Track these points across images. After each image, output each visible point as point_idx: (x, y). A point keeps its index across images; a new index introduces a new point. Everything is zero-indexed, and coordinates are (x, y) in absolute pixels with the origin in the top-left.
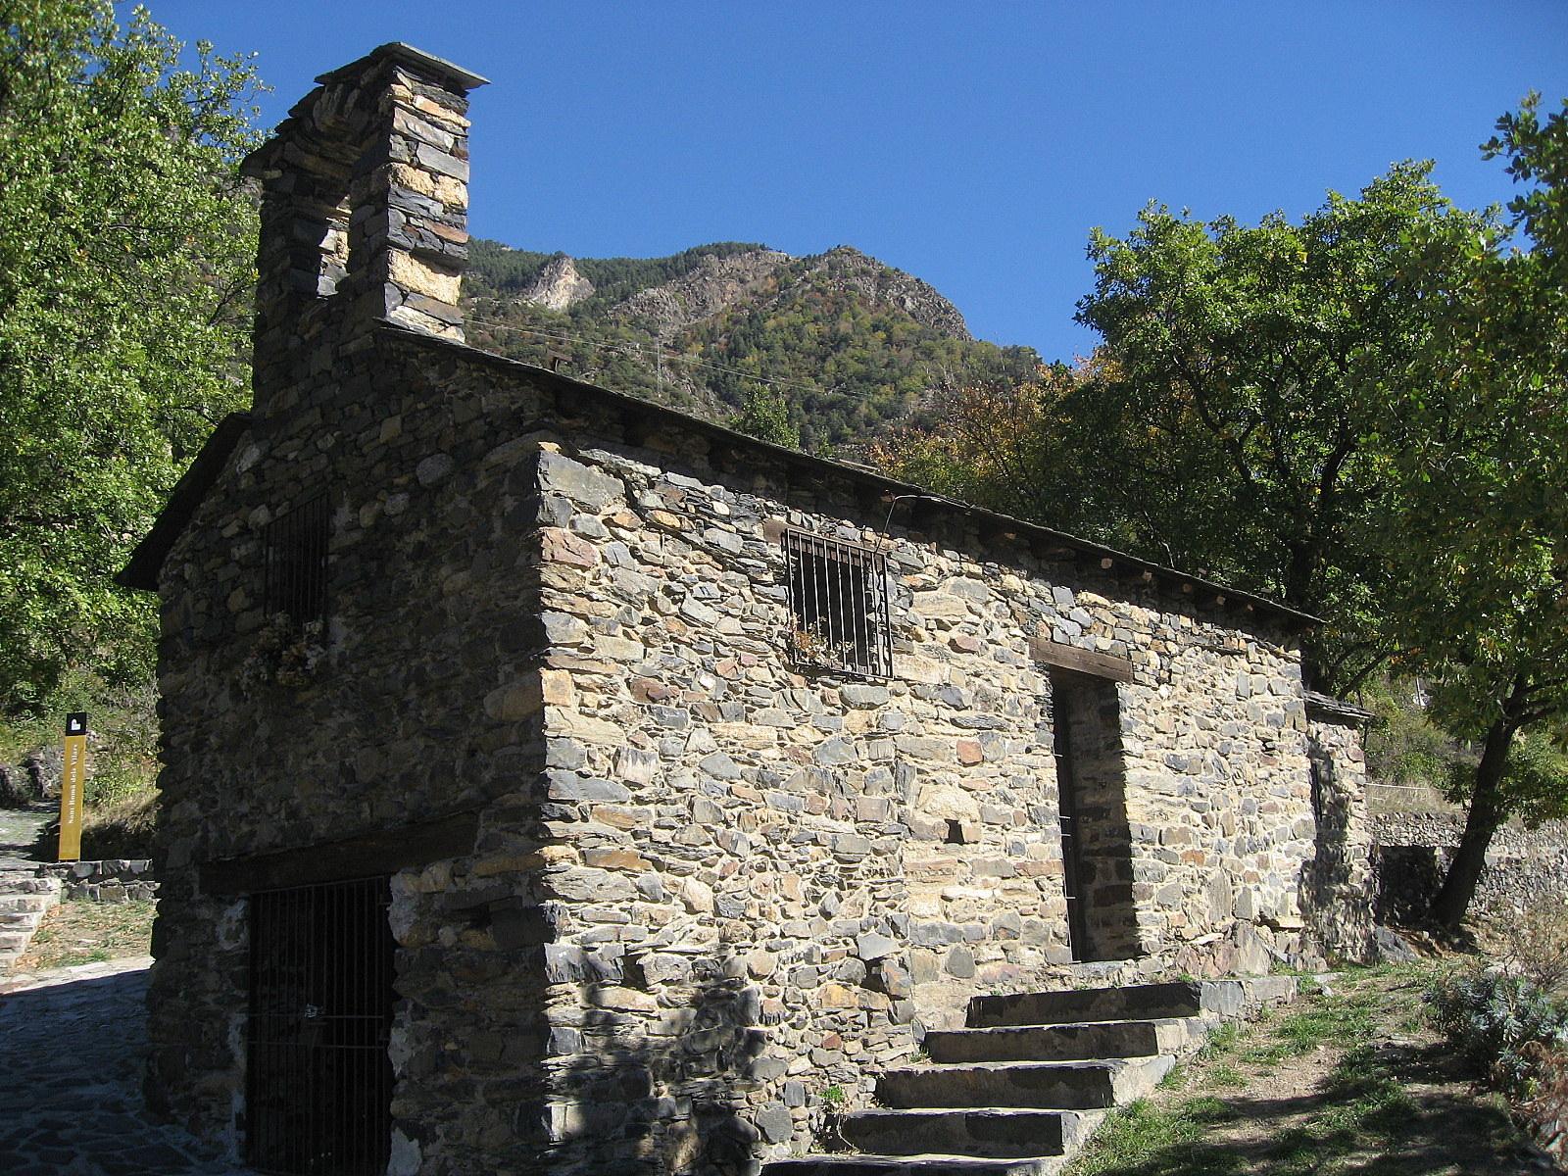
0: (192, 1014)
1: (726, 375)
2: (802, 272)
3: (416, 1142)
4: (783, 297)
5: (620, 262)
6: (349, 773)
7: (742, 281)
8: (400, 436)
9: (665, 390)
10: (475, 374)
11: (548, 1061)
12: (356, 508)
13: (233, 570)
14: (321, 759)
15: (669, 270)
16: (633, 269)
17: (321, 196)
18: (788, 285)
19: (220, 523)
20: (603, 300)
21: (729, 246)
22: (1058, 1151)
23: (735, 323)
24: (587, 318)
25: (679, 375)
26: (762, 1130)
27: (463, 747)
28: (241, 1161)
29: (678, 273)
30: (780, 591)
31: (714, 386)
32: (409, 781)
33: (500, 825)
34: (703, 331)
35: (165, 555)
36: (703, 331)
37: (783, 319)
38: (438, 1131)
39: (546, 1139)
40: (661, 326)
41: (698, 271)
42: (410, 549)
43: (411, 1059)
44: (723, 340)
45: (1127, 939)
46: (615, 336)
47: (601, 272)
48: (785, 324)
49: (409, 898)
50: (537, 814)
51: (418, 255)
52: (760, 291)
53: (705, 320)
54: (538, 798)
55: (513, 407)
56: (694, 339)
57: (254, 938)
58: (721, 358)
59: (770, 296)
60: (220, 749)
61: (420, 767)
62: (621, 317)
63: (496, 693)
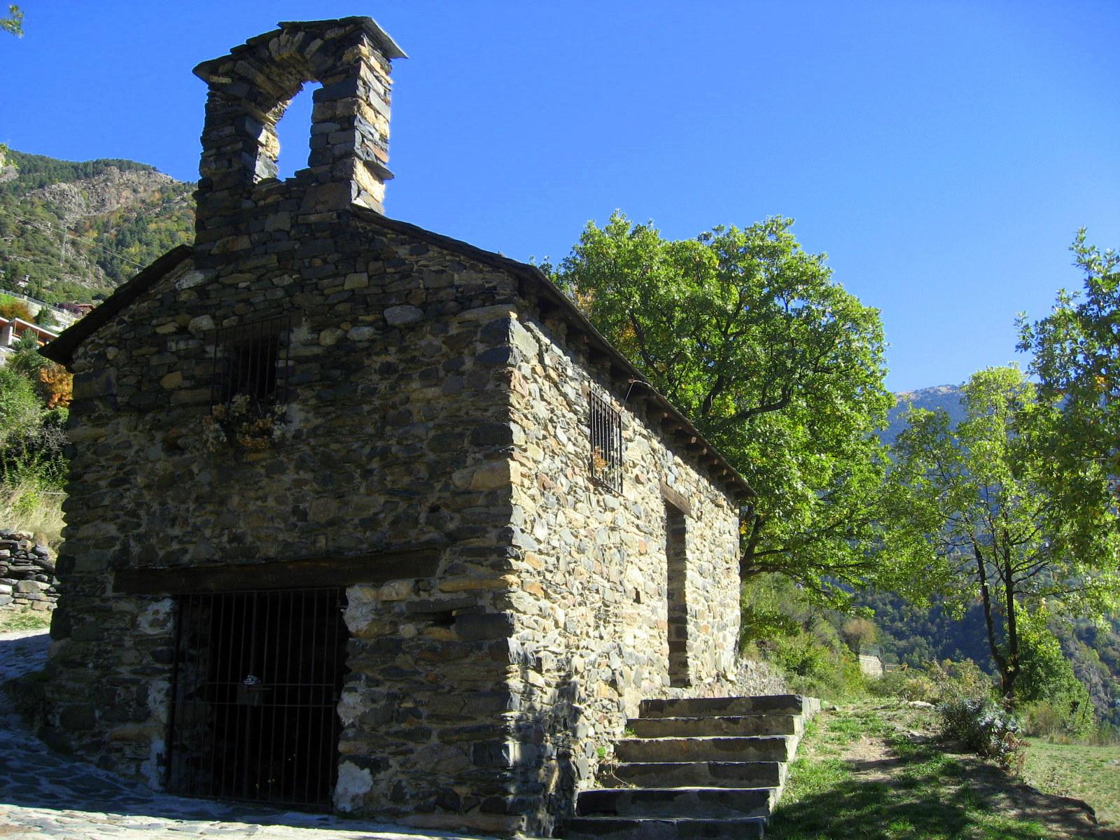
0: (104, 680)
1: (113, 258)
2: (181, 193)
3: (367, 771)
4: (165, 208)
5: (42, 159)
6: (303, 515)
7: (135, 191)
8: (366, 288)
9: (67, 261)
10: (448, 258)
11: (507, 714)
12: (317, 329)
13: (169, 359)
14: (271, 502)
15: (79, 172)
16: (51, 166)
17: (259, 105)
18: (169, 201)
19: (154, 322)
20: (24, 184)
21: (129, 163)
22: (778, 785)
23: (125, 221)
24: (11, 195)
25: (78, 252)
26: (578, 770)
27: (427, 504)
28: (160, 788)
29: (86, 175)
30: (587, 431)
31: (103, 265)
32: (370, 523)
33: (464, 558)
34: (100, 222)
35: (87, 337)
36: (100, 222)
37: (162, 225)
38: (391, 762)
39: (504, 765)
40: (67, 213)
41: (102, 177)
42: (377, 366)
43: (364, 715)
44: (113, 232)
45: (681, 676)
46: (32, 214)
47: (26, 163)
48: (163, 228)
49: (365, 604)
50: (502, 553)
51: (367, 165)
52: (148, 201)
53: (102, 215)
54: (502, 544)
55: (487, 286)
56: (91, 227)
57: (178, 627)
58: (111, 245)
59: (155, 206)
60: (148, 487)
61: (382, 515)
62: (36, 200)
63: (465, 472)
